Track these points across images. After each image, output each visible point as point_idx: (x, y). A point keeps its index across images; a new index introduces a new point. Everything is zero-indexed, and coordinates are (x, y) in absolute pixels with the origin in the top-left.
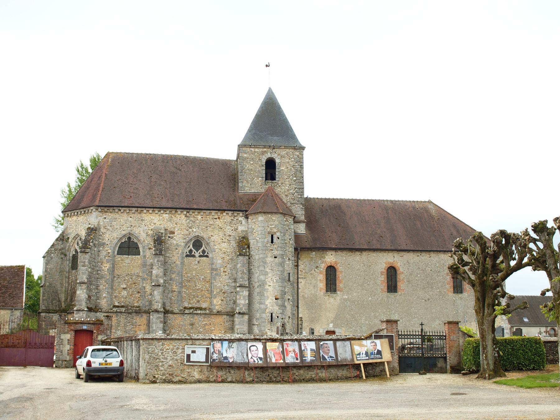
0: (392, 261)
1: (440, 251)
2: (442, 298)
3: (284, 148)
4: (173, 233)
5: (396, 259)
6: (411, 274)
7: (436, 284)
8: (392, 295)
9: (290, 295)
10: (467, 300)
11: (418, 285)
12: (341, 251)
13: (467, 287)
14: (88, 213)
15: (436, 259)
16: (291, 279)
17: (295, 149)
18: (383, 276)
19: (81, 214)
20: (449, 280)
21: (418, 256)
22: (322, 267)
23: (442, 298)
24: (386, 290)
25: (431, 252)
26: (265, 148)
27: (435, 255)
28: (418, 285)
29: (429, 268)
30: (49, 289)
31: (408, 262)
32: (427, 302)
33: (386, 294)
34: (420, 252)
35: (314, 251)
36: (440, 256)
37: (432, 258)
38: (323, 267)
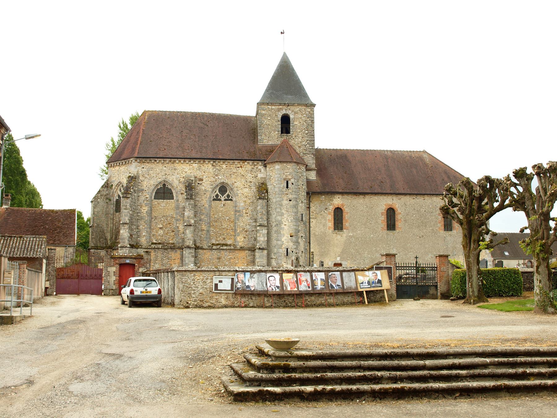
0: (391, 203)
8: (391, 233)
15: (430, 201)
16: (304, 219)
17: (307, 106)
18: (383, 216)
20: (440, 219)
21: (414, 199)
26: (280, 105)
28: (413, 224)
29: (423, 209)
32: (421, 238)
33: (386, 231)
35: (323, 195)
36: (433, 199)
37: (426, 201)
38: (331, 208)
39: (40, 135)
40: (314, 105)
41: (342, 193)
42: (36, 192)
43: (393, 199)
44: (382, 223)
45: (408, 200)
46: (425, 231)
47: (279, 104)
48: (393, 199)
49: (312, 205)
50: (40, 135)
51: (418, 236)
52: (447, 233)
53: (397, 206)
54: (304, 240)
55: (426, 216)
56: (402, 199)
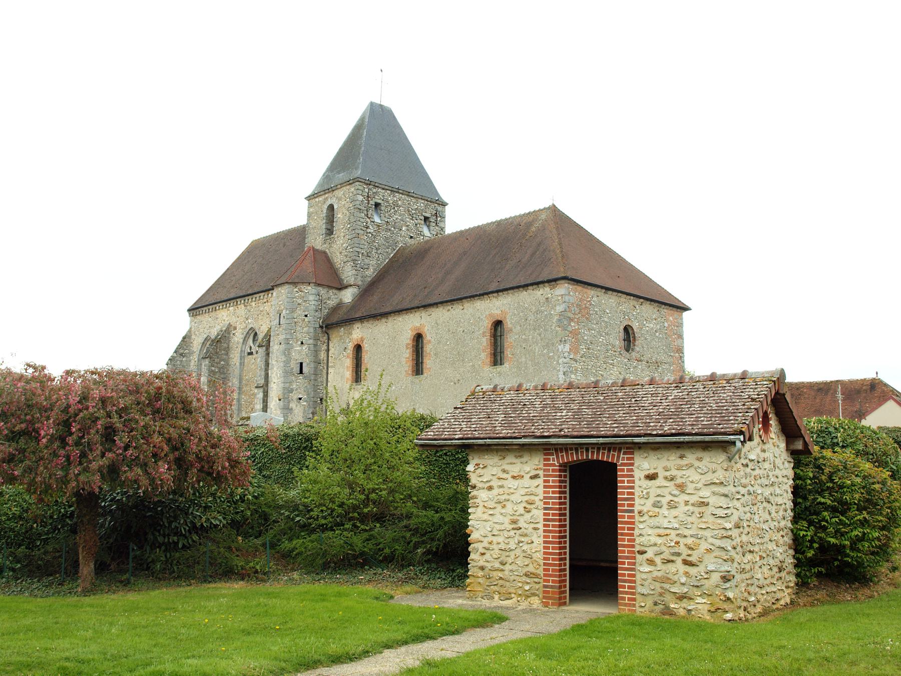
0: (418, 325)
1: (454, 300)
2: (476, 375)
3: (341, 187)
4: (235, 328)
5: (423, 321)
6: (439, 342)
7: (469, 353)
8: (417, 379)
9: (302, 392)
10: (508, 375)
11: (447, 358)
12: (367, 321)
13: (509, 353)
14: (208, 312)
15: (471, 310)
16: (305, 370)
17: (350, 184)
18: (408, 351)
19: (208, 312)
20: (485, 344)
21: (449, 310)
22: (350, 347)
23: (476, 375)
24: (410, 372)
25: (463, 301)
26: (325, 193)
27: (469, 304)
28: (447, 358)
29: (461, 327)
30: (782, 543)
31: (436, 323)
32: (457, 385)
33: (410, 378)
34: (449, 304)
35: (342, 326)
36: (475, 305)
37: (465, 310)
38: (351, 346)
39: (418, 368)
40: (444, 204)
41: (361, 319)
42: (149, 383)
43: (421, 317)
44: (406, 363)
45: (440, 314)
46: (462, 369)
47: (323, 193)
48: (421, 317)
49: (331, 345)
50: (418, 368)
51: (451, 381)
52: (495, 370)
53: (426, 328)
54: (305, 403)
55: (465, 340)
56: (433, 314)
